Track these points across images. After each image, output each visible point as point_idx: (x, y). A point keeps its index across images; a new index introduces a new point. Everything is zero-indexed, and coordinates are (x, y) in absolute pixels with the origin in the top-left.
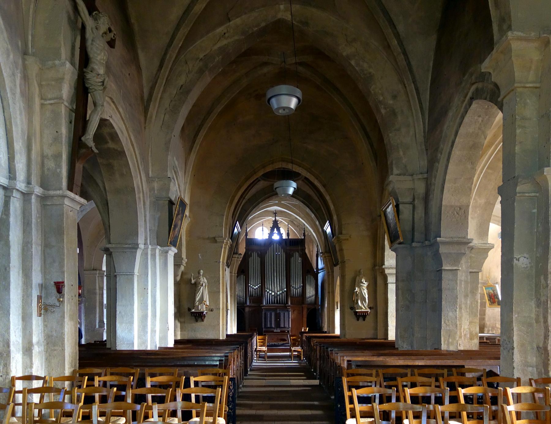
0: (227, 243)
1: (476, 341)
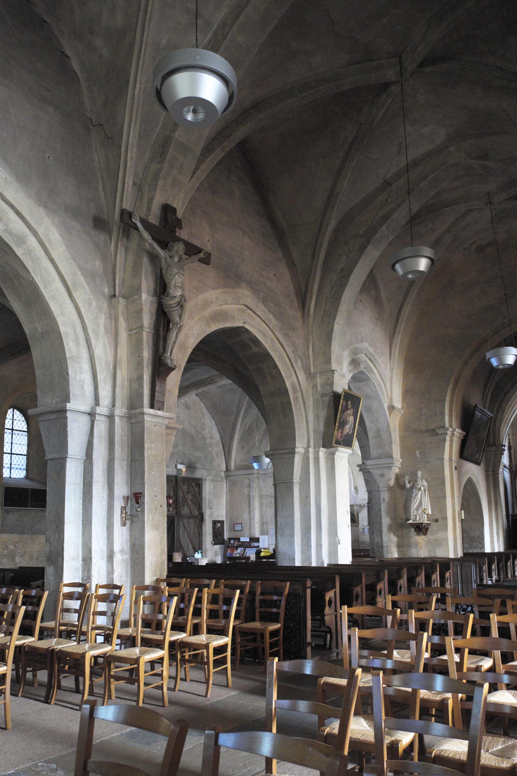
0: (453, 434)
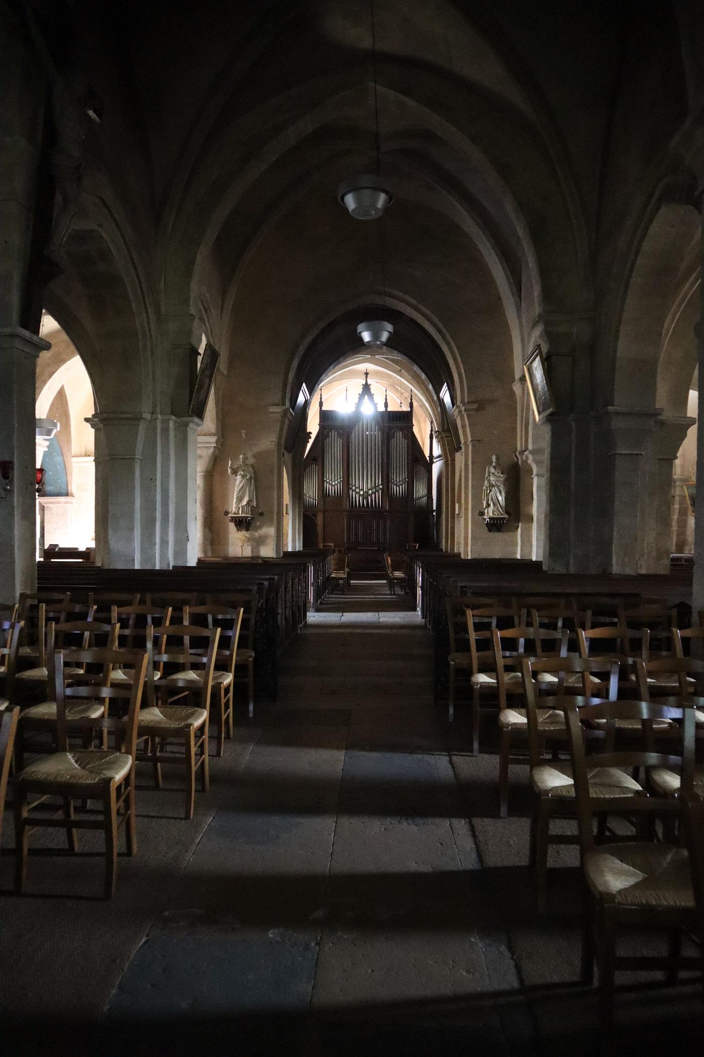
1: (666, 562)
